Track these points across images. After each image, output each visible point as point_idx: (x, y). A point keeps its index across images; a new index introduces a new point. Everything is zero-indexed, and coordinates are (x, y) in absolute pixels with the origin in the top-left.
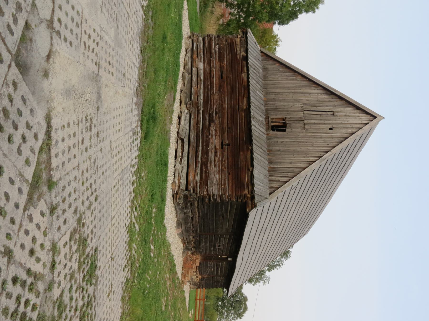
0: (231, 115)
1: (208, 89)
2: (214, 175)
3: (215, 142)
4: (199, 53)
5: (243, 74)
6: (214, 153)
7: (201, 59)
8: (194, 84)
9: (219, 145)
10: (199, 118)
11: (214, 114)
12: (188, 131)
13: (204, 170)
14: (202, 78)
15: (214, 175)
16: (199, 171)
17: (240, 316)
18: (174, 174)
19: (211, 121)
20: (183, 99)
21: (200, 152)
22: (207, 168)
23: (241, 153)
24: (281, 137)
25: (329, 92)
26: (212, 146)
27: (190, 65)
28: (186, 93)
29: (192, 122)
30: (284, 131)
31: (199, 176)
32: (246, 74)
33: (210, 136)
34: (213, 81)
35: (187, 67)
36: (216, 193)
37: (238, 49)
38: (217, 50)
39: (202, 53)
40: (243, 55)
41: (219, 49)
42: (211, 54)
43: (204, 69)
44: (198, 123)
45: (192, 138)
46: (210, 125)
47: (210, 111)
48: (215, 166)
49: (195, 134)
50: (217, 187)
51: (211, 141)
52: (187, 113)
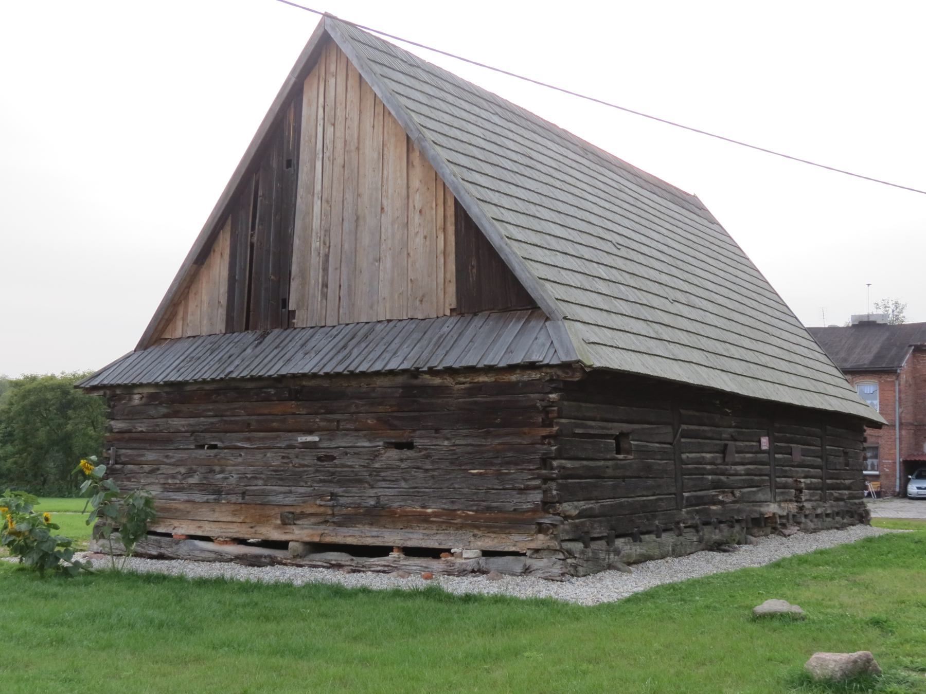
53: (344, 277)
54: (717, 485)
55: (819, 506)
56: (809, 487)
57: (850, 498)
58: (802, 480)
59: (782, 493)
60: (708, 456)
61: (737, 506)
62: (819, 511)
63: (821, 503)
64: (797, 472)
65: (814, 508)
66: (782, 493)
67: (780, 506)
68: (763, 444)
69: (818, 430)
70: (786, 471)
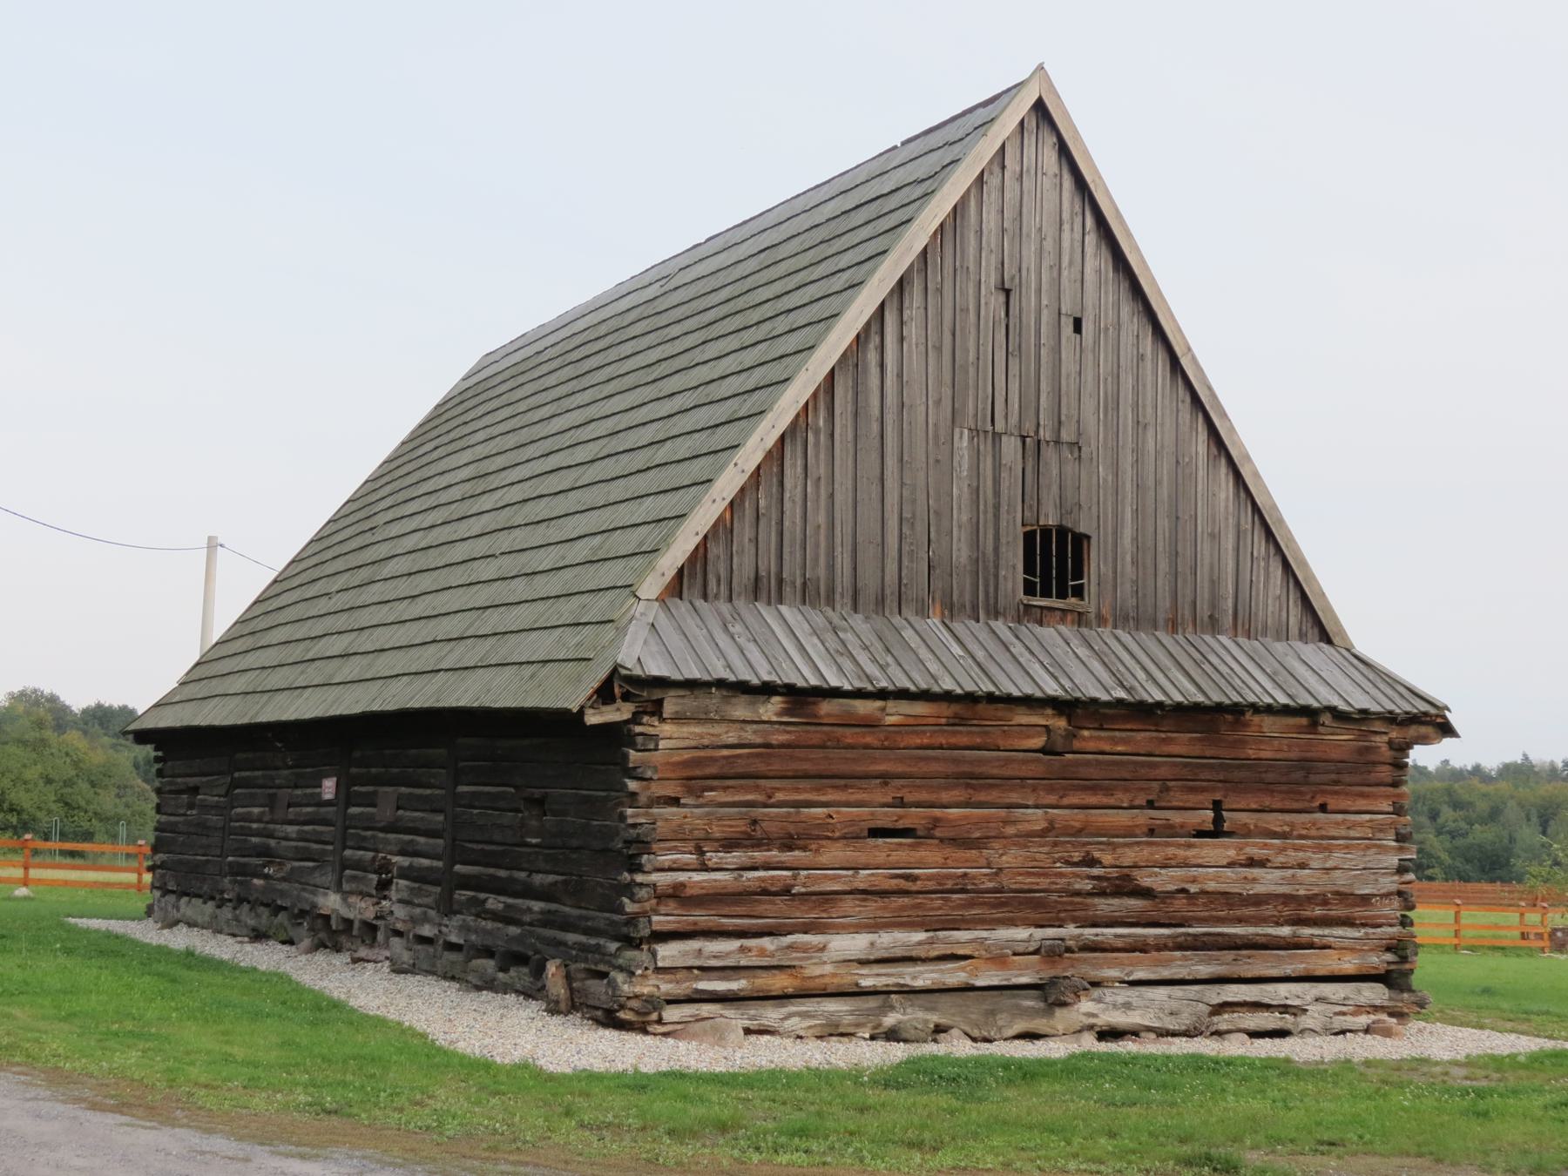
0: (1094, 789)
1: (971, 904)
2: (1336, 868)
3: (1213, 866)
4: (765, 962)
5: (890, 720)
6: (1256, 872)
7: (805, 948)
8: (954, 975)
9: (1227, 847)
10: (1119, 943)
11: (1096, 871)
12: (1177, 991)
13: (1318, 912)
14: (921, 936)
15: (1336, 868)
16: (1327, 931)
17: (1446, 762)
18: (1343, 1032)
19: (1124, 886)
20: (1020, 1026)
21: (1259, 930)
22: (1310, 899)
23: (1251, 753)
24: (1115, 560)
25: (745, 222)
26: (1230, 882)
27: (831, 1006)
28: (992, 1013)
29: (1140, 974)
30: (1081, 540)
31: (1339, 931)
32: (891, 705)
33: (1193, 889)
34: (930, 878)
35: (848, 1019)
36: (1394, 861)
37: (731, 738)
38: (736, 857)
39: (767, 943)
40: (779, 714)
41: (729, 844)
42: (765, 892)
43: (858, 928)
44: (1141, 947)
45: (1204, 970)
46: (1146, 893)
47: (1078, 893)
48: (1302, 866)
49: (1186, 958)
50: (1372, 858)
51: (1212, 886)
52: (1099, 1001)
53: (1151, 1047)
54: (265, 852)
55: (425, 919)
56: (405, 873)
57: (546, 924)
58: (395, 859)
59: (354, 878)
60: (256, 810)
61: (284, 886)
62: (427, 931)
63: (432, 913)
64: (387, 842)
65: (413, 920)
66: (354, 878)
67: (344, 900)
68: (333, 790)
69: (442, 751)
70: (364, 838)
